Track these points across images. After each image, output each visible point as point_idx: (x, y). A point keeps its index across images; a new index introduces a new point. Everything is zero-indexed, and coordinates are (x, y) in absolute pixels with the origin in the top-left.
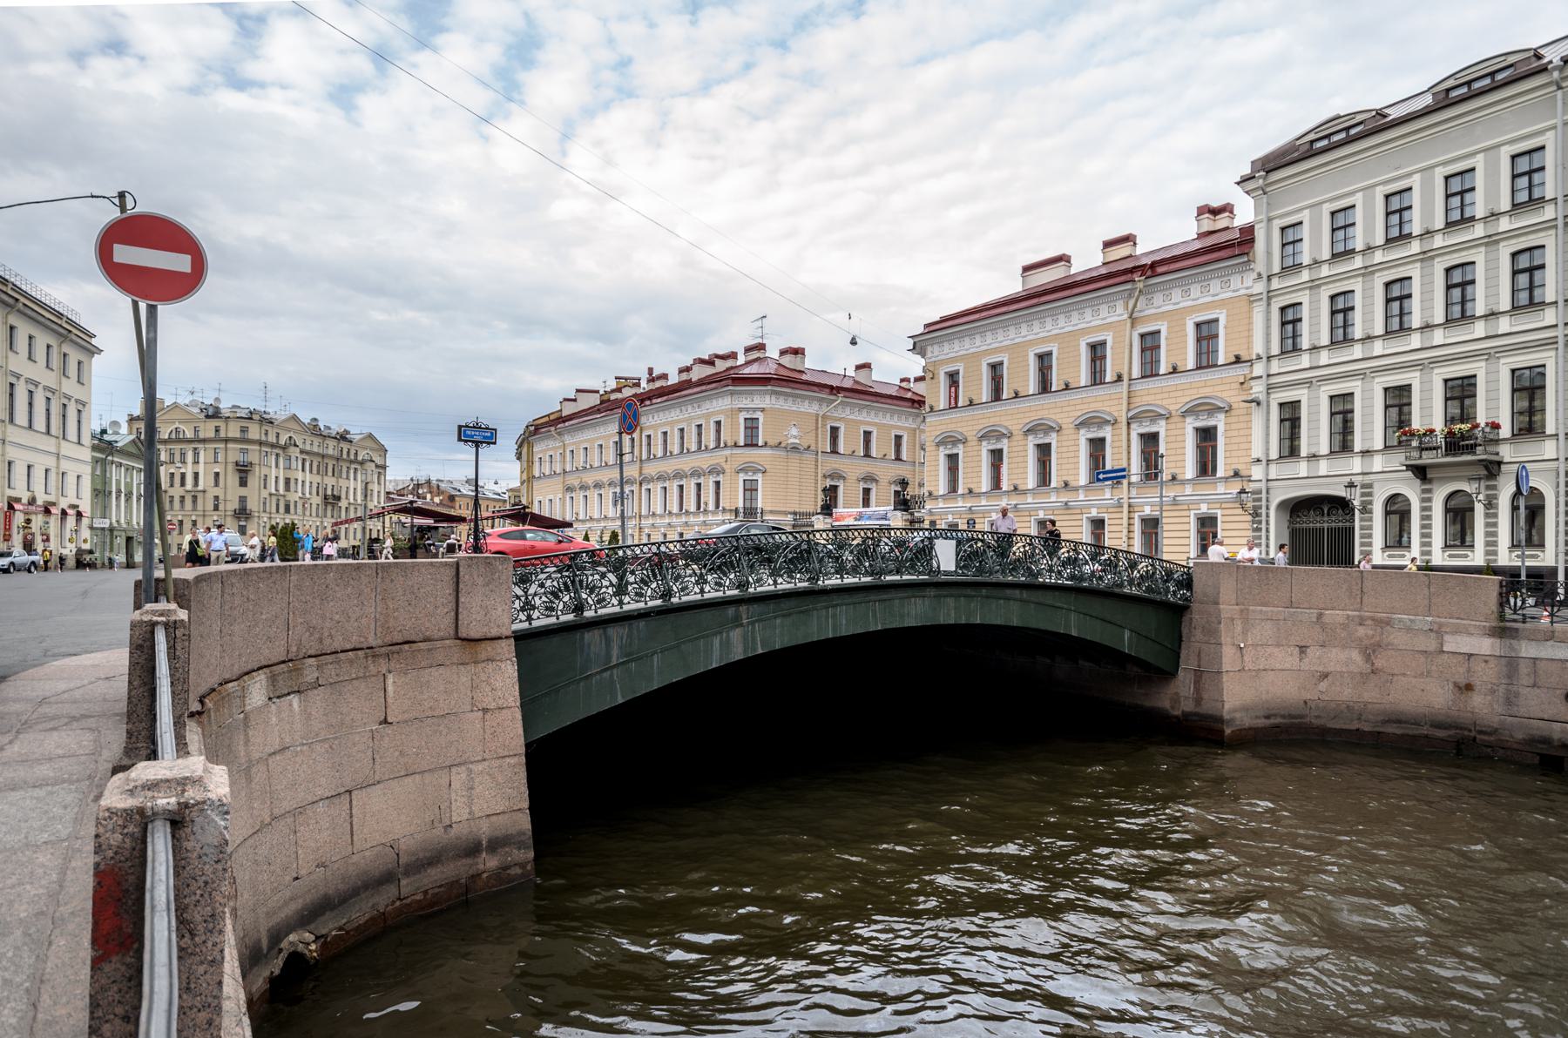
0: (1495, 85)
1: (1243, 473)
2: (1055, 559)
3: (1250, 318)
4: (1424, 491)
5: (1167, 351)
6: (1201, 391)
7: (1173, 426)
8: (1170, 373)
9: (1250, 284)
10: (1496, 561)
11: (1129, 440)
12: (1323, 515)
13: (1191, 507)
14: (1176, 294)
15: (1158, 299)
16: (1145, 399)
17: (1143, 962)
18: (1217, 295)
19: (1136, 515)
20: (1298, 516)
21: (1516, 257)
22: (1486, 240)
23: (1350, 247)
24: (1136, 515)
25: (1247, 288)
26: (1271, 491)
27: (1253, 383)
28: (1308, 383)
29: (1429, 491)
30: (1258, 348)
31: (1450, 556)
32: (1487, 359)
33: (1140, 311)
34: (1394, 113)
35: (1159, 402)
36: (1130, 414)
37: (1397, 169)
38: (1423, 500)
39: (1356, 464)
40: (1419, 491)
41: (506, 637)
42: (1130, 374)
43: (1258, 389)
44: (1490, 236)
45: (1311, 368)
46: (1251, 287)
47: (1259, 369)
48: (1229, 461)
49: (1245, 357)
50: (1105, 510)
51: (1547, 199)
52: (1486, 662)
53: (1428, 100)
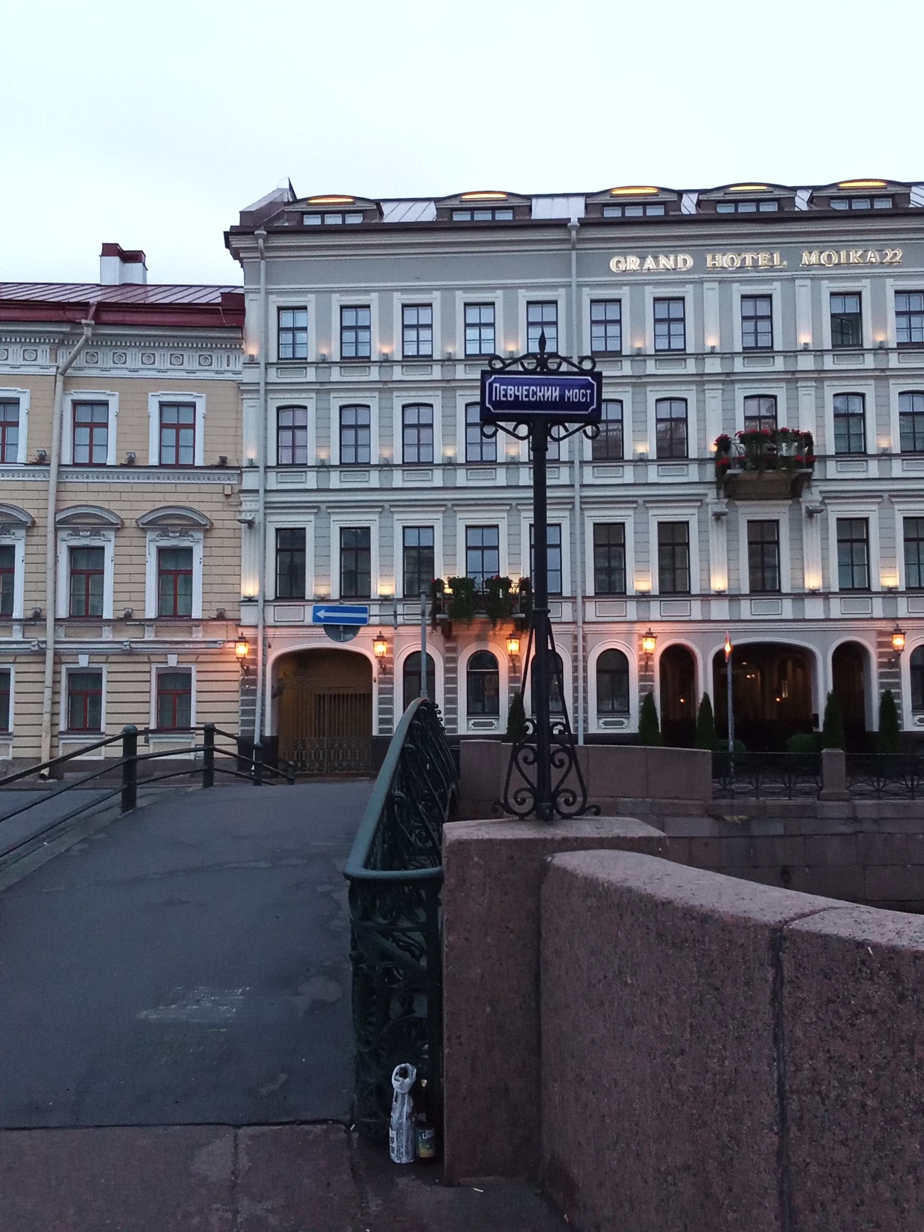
0: (782, 215)
1: (229, 615)
3: (239, 412)
4: (448, 650)
5: (118, 434)
6: (169, 497)
7: (126, 541)
8: (123, 466)
9: (239, 367)
10: (455, 730)
11: (56, 556)
13: (153, 658)
14: (134, 359)
15: (106, 359)
16: (81, 496)
18: (193, 372)
19: (63, 668)
21: (343, 411)
22: (444, 385)
23: (364, 352)
24: (63, 668)
25: (235, 373)
26: (589, 638)
27: (243, 497)
28: (315, 507)
29: (453, 650)
30: (251, 453)
31: (605, 723)
32: (444, 512)
33: (76, 369)
34: (392, 215)
35: (106, 505)
36: (60, 516)
37: (418, 279)
38: (447, 660)
40: (442, 650)
42: (59, 456)
43: (251, 507)
44: (322, 383)
45: (318, 490)
46: (240, 373)
47: (250, 481)
48: (210, 597)
49: (231, 462)
50: (193, 658)
51: (309, 360)
52: (707, 845)
53: (429, 214)
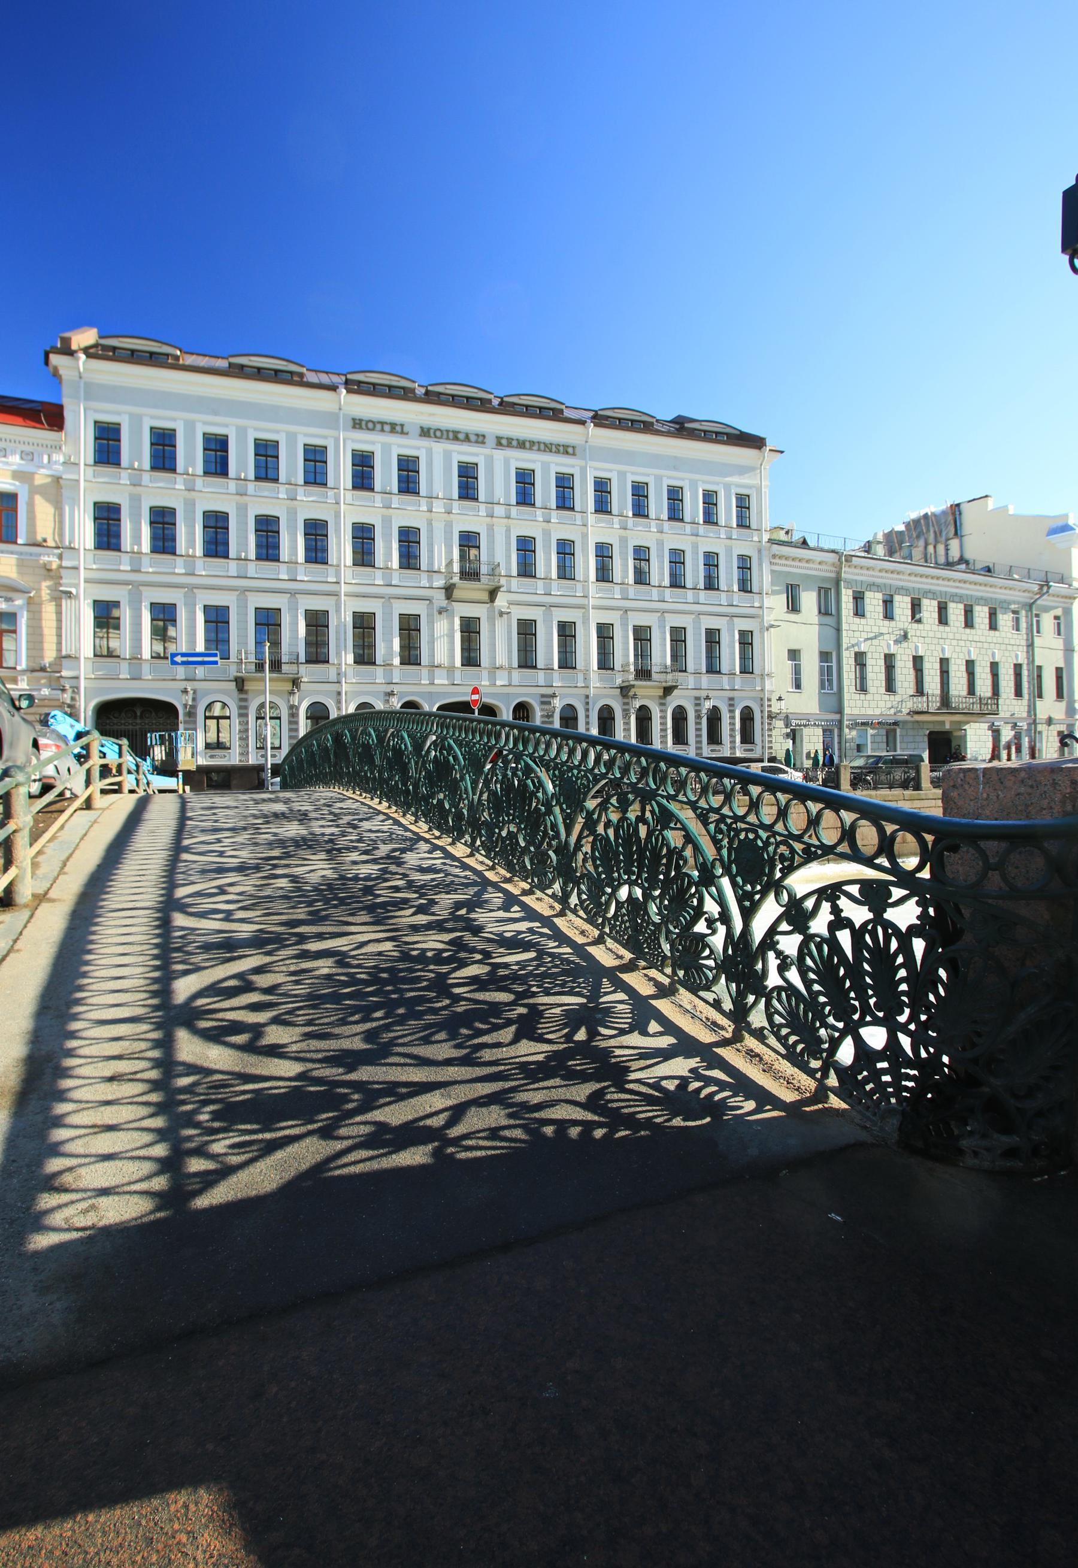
2: (769, 911)
4: (241, 700)
12: (135, 717)
17: (471, 1139)
20: (109, 718)
29: (245, 700)
38: (240, 707)
39: (541, 677)
40: (621, 703)
41: (1031, 646)
